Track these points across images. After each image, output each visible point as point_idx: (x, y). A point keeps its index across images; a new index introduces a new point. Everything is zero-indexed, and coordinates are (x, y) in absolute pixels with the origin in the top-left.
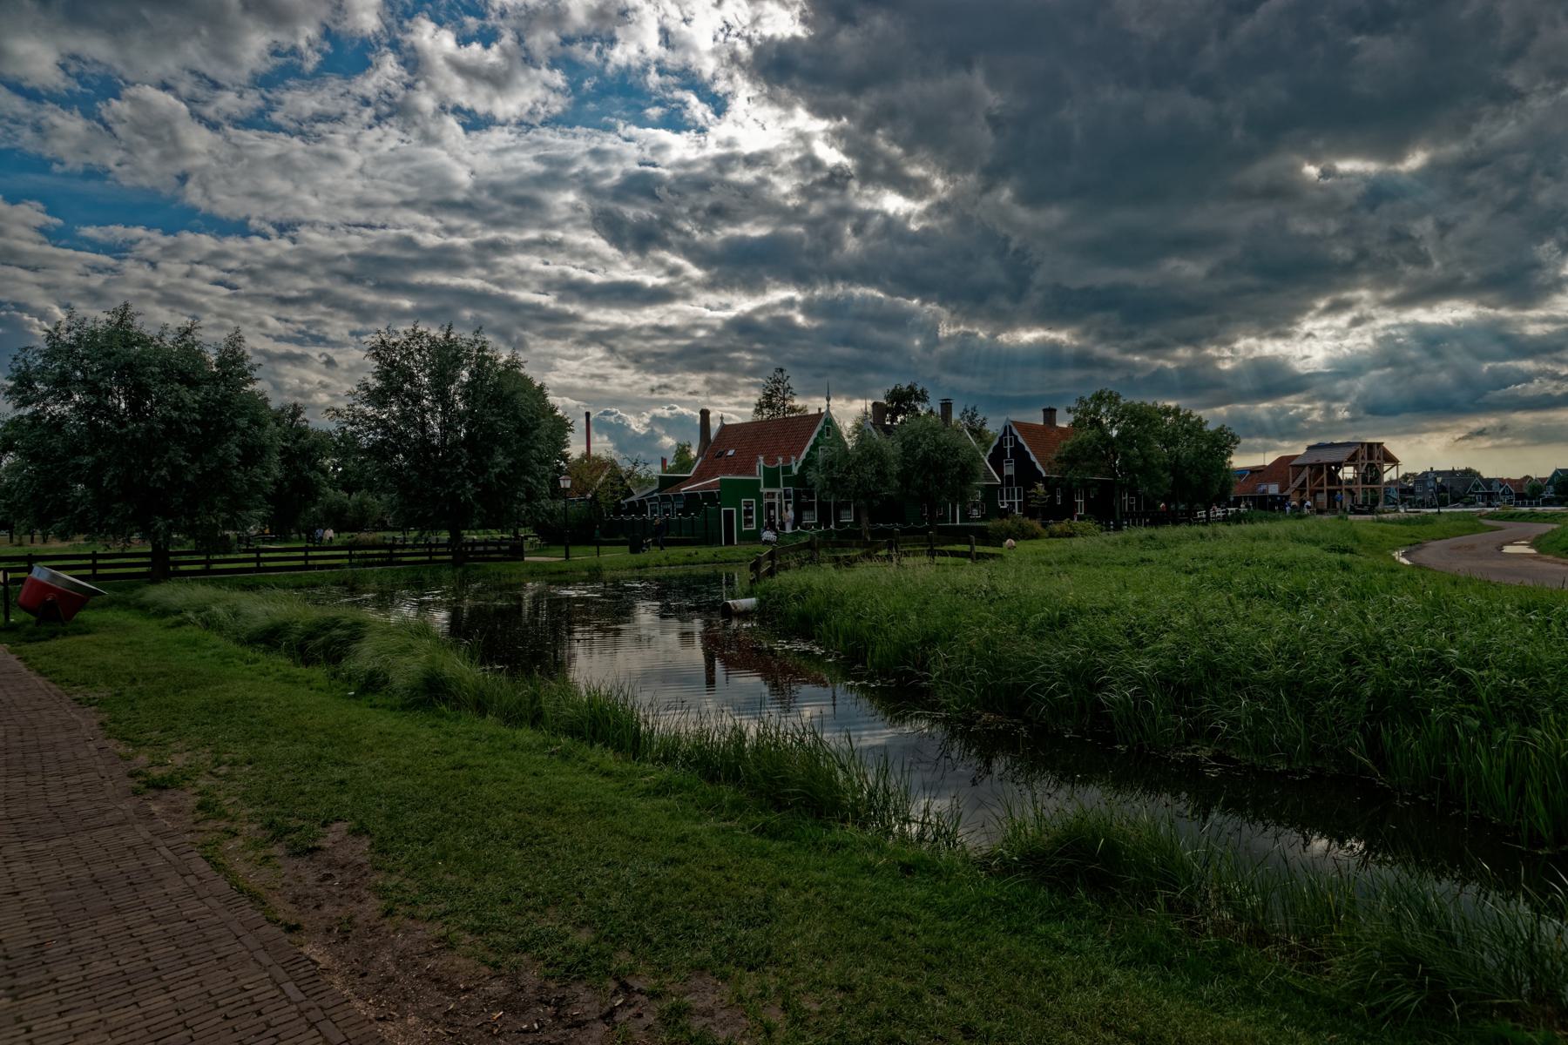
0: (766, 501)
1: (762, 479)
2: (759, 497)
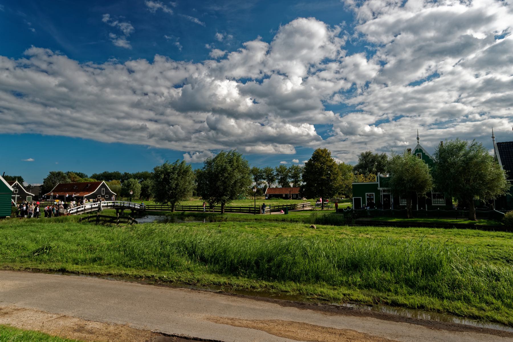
0: (382, 194)
1: (379, 183)
2: (378, 192)
